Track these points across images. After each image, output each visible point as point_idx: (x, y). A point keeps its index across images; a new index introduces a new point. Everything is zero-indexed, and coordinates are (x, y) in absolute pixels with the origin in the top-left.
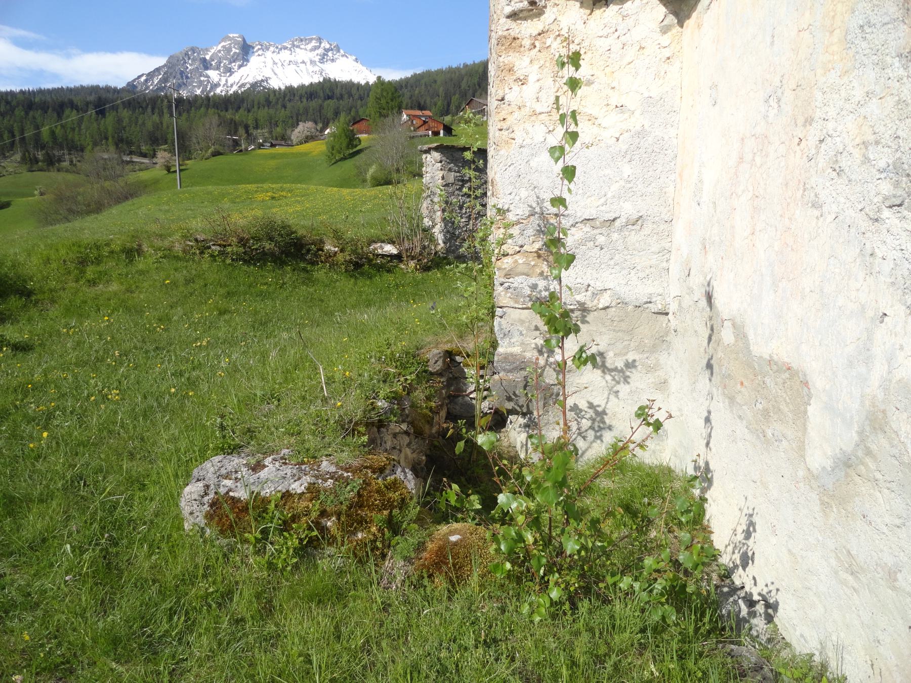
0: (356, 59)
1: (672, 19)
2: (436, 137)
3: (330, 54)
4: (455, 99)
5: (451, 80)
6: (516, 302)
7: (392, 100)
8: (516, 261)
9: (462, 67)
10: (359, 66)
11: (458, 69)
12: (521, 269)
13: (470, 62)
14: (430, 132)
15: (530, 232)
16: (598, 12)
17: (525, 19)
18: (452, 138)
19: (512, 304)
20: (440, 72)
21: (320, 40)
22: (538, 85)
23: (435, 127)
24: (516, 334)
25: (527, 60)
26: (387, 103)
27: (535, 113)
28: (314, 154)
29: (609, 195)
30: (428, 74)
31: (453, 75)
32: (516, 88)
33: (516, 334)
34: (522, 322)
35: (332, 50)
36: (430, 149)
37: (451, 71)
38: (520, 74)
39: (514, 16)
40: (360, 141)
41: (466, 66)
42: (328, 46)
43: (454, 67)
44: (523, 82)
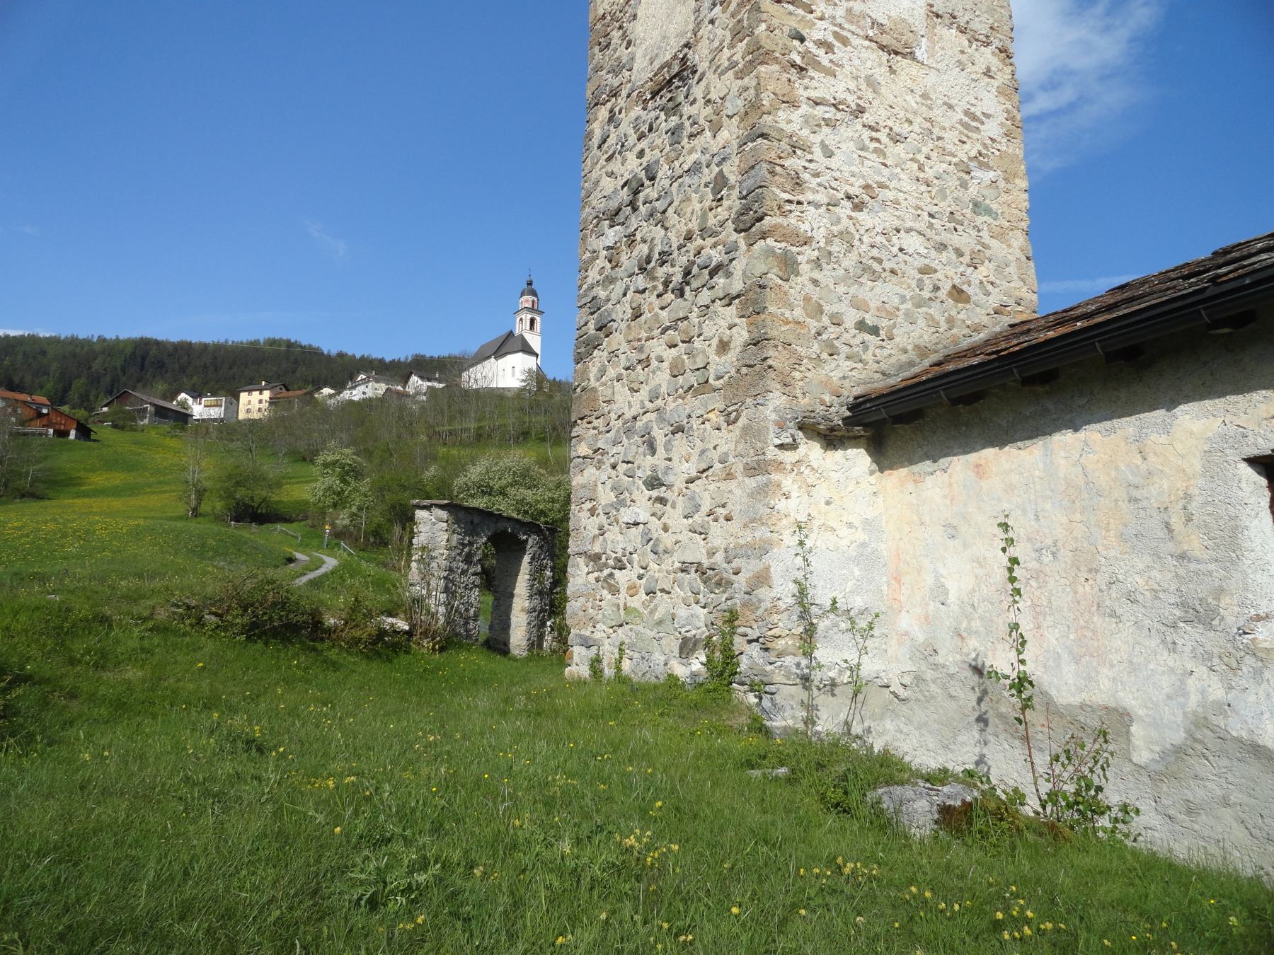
1: (875, 466)
2: (62, 439)
4: (79, 384)
5: (75, 355)
6: (789, 679)
8: (787, 643)
9: (95, 340)
11: (87, 342)
12: (791, 649)
13: (110, 335)
14: (51, 431)
15: (795, 618)
16: (830, 453)
17: (787, 450)
18: (92, 443)
19: (784, 681)
22: (798, 500)
24: (788, 708)
25: (790, 481)
29: (848, 590)
30: (33, 339)
31: (78, 350)
32: (783, 499)
33: (788, 708)
34: (792, 696)
36: (432, 505)
37: (73, 341)
38: (785, 490)
39: (781, 447)
41: (102, 340)
43: (81, 337)
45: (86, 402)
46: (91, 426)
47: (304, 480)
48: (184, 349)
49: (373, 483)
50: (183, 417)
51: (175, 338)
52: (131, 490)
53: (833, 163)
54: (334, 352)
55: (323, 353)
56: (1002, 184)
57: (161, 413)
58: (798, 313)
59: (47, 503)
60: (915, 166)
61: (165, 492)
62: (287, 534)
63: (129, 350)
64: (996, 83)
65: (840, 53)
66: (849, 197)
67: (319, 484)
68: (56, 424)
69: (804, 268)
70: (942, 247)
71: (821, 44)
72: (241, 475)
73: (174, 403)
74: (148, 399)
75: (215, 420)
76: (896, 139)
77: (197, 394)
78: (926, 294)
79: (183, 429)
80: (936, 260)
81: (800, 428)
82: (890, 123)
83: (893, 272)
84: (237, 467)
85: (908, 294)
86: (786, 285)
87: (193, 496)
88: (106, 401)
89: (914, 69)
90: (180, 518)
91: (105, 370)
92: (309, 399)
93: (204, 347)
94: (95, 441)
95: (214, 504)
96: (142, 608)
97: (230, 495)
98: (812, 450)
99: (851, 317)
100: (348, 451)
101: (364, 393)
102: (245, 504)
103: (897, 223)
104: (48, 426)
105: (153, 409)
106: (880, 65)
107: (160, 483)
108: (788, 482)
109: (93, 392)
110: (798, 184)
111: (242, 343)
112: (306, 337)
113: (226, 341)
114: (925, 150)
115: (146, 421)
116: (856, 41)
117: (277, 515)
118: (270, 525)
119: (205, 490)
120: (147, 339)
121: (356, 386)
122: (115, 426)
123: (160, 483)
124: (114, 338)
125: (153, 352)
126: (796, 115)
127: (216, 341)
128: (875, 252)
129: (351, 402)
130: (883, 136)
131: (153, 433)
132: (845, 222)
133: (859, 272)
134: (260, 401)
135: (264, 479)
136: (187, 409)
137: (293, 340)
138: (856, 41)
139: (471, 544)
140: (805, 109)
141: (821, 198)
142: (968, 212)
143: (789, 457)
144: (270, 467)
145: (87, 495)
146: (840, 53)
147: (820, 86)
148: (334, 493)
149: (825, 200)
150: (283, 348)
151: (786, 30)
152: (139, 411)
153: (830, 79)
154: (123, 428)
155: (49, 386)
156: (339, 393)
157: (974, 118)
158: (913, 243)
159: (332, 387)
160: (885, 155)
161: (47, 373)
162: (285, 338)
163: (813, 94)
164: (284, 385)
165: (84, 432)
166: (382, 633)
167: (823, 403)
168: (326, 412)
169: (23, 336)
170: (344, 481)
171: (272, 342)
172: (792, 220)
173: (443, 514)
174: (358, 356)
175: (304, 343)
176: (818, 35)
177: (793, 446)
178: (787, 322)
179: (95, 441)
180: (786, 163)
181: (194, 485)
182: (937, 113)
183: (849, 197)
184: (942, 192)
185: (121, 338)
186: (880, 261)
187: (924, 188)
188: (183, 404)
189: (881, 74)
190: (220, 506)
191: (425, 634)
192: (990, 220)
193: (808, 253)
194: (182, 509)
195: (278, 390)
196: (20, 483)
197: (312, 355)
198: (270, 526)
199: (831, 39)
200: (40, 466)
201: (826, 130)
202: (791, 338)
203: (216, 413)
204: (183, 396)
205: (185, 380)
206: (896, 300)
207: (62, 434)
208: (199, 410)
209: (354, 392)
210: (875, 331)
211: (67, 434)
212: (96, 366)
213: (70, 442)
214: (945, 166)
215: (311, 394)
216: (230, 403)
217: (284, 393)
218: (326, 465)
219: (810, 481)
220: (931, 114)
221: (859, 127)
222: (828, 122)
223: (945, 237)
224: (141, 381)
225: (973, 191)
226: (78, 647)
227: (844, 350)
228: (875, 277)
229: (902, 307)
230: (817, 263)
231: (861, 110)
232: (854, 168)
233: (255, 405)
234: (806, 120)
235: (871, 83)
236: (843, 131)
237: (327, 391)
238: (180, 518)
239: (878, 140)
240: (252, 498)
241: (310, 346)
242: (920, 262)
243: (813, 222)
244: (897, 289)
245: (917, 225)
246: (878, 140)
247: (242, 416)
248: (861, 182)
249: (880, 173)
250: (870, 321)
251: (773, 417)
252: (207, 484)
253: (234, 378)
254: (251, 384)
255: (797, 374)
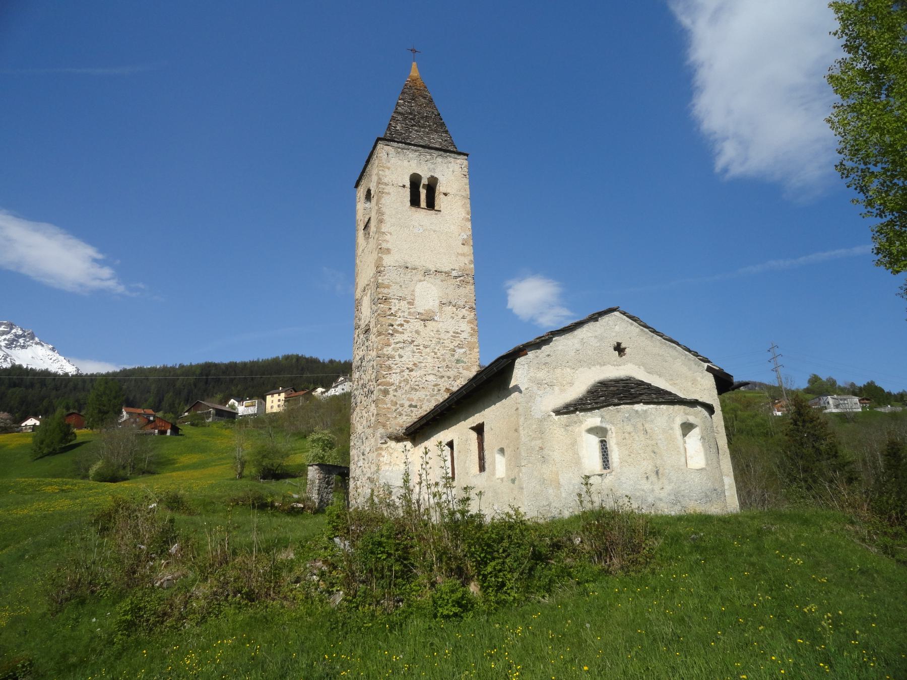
0: (53, 348)
2: (163, 436)
3: (21, 341)
7: (115, 398)
9: (177, 367)
10: (56, 355)
11: (173, 369)
13: (186, 363)
14: (156, 431)
18: (180, 437)
20: (153, 370)
21: (11, 326)
23: (162, 426)
26: (109, 400)
27: (386, 463)
28: (11, 447)
30: (140, 370)
35: (24, 336)
37: (165, 369)
39: (382, 443)
40: (75, 436)
41: (182, 366)
42: (20, 332)
43: (169, 366)
44: (384, 457)
45: (173, 409)
46: (178, 425)
47: (304, 450)
48: (232, 368)
49: (338, 451)
50: (232, 415)
51: (226, 361)
52: (203, 465)
53: (403, 359)
54: (327, 360)
55: (319, 361)
56: (468, 352)
57: (220, 413)
58: (389, 405)
59: (157, 476)
60: (433, 354)
61: (222, 464)
62: (292, 485)
63: (198, 372)
64: (466, 320)
65: (406, 326)
66: (408, 369)
67: (310, 453)
68: (159, 426)
69: (391, 392)
70: (442, 377)
71: (398, 325)
72: (265, 451)
73: (227, 406)
74: (211, 405)
75: (252, 415)
76: (425, 347)
77: (241, 400)
78: (435, 393)
79: (233, 423)
80: (440, 381)
81: (388, 438)
82: (424, 343)
83: (423, 388)
84: (263, 446)
85: (428, 394)
86: (385, 398)
87: (239, 466)
88: (186, 409)
89: (433, 323)
90: (232, 479)
91: (184, 386)
92: (309, 395)
93: (244, 365)
94: (181, 435)
95: (251, 470)
96: (223, 500)
97: (260, 464)
98: (392, 444)
99: (407, 404)
100: (326, 432)
101: (343, 389)
102: (268, 469)
103: (425, 373)
104: (155, 428)
105: (214, 412)
106: (421, 326)
107: (220, 459)
108: (383, 453)
109: (177, 401)
110: (390, 368)
111: (268, 360)
112: (308, 352)
113: (258, 359)
114: (437, 348)
115: (210, 420)
116: (411, 321)
117: (287, 474)
118: (282, 480)
119: (245, 462)
120: (209, 363)
121: (338, 385)
122: (192, 425)
123: (220, 459)
124: (189, 364)
125: (213, 371)
126: (390, 349)
127: (252, 360)
128: (417, 383)
129: (335, 397)
130: (421, 347)
131: (215, 426)
132: (406, 376)
133: (410, 390)
134: (279, 400)
135: (279, 452)
136: (234, 409)
137: (300, 355)
138: (411, 321)
139: (328, 477)
140: (393, 346)
141: (398, 371)
142: (454, 364)
143: (384, 446)
144: (282, 443)
145: (178, 469)
146: (406, 326)
147: (399, 337)
148: (319, 458)
149: (399, 371)
150: (294, 360)
151: (387, 324)
152: (207, 413)
153: (403, 335)
154: (197, 425)
155: (151, 400)
156: (327, 391)
157: (457, 333)
158: (431, 378)
159: (323, 387)
160: (421, 353)
161: (149, 392)
162: (295, 354)
163: (395, 341)
164: (293, 389)
165: (175, 430)
166: (293, 508)
167: (396, 429)
168: (319, 404)
169: (134, 369)
170: (324, 450)
171: (287, 358)
172: (388, 379)
173: (316, 467)
174: (342, 362)
175: (307, 356)
176: (398, 323)
177: (386, 443)
178: (385, 408)
179: (181, 435)
180: (386, 363)
181: (239, 459)
182: (442, 336)
183: (408, 369)
184: (444, 360)
185: (193, 364)
186: (418, 385)
187: (436, 360)
188: (232, 406)
189: (421, 328)
190: (254, 470)
191: (309, 508)
192: (462, 364)
193: (393, 387)
194: (233, 474)
195: (289, 392)
196: (141, 465)
197: (312, 363)
198: (283, 481)
199: (403, 323)
200: (152, 453)
201: (400, 350)
202: (386, 413)
203: (252, 410)
204: (232, 401)
205: (233, 388)
206: (424, 396)
207: (163, 432)
208: (243, 409)
209: (337, 389)
210: (416, 407)
211: (165, 432)
212: (178, 384)
213: (167, 437)
214: (445, 351)
215: (310, 393)
216: (260, 404)
217: (294, 394)
218: (313, 441)
219: (391, 452)
220: (440, 336)
221: (412, 346)
222: (401, 348)
223: (444, 374)
224: (207, 393)
225: (456, 357)
226: (209, 508)
227: (405, 413)
228: (416, 390)
229: (426, 398)
230: (396, 390)
231: (413, 341)
232: (410, 360)
233: (276, 403)
234: (393, 349)
235: (417, 332)
236: (407, 349)
237: (320, 390)
238: (232, 479)
239: (419, 349)
240: (272, 465)
241: (311, 357)
242: (433, 383)
243: (395, 379)
244: (424, 393)
245: (433, 372)
246: (419, 349)
247: (269, 410)
248: (413, 363)
249: (419, 359)
250: (414, 404)
251: (379, 435)
252: (247, 458)
253: (263, 384)
254: (273, 389)
255: (388, 423)
